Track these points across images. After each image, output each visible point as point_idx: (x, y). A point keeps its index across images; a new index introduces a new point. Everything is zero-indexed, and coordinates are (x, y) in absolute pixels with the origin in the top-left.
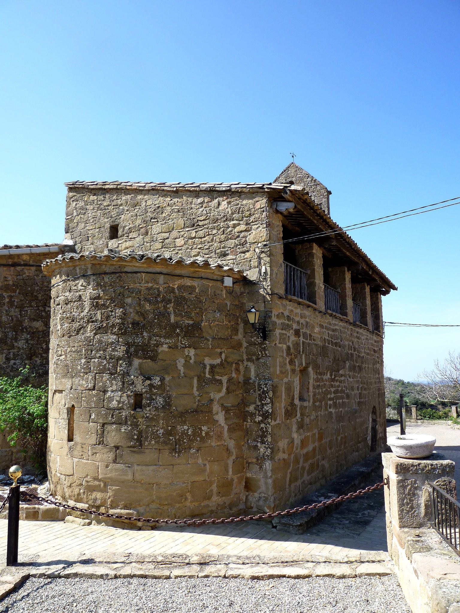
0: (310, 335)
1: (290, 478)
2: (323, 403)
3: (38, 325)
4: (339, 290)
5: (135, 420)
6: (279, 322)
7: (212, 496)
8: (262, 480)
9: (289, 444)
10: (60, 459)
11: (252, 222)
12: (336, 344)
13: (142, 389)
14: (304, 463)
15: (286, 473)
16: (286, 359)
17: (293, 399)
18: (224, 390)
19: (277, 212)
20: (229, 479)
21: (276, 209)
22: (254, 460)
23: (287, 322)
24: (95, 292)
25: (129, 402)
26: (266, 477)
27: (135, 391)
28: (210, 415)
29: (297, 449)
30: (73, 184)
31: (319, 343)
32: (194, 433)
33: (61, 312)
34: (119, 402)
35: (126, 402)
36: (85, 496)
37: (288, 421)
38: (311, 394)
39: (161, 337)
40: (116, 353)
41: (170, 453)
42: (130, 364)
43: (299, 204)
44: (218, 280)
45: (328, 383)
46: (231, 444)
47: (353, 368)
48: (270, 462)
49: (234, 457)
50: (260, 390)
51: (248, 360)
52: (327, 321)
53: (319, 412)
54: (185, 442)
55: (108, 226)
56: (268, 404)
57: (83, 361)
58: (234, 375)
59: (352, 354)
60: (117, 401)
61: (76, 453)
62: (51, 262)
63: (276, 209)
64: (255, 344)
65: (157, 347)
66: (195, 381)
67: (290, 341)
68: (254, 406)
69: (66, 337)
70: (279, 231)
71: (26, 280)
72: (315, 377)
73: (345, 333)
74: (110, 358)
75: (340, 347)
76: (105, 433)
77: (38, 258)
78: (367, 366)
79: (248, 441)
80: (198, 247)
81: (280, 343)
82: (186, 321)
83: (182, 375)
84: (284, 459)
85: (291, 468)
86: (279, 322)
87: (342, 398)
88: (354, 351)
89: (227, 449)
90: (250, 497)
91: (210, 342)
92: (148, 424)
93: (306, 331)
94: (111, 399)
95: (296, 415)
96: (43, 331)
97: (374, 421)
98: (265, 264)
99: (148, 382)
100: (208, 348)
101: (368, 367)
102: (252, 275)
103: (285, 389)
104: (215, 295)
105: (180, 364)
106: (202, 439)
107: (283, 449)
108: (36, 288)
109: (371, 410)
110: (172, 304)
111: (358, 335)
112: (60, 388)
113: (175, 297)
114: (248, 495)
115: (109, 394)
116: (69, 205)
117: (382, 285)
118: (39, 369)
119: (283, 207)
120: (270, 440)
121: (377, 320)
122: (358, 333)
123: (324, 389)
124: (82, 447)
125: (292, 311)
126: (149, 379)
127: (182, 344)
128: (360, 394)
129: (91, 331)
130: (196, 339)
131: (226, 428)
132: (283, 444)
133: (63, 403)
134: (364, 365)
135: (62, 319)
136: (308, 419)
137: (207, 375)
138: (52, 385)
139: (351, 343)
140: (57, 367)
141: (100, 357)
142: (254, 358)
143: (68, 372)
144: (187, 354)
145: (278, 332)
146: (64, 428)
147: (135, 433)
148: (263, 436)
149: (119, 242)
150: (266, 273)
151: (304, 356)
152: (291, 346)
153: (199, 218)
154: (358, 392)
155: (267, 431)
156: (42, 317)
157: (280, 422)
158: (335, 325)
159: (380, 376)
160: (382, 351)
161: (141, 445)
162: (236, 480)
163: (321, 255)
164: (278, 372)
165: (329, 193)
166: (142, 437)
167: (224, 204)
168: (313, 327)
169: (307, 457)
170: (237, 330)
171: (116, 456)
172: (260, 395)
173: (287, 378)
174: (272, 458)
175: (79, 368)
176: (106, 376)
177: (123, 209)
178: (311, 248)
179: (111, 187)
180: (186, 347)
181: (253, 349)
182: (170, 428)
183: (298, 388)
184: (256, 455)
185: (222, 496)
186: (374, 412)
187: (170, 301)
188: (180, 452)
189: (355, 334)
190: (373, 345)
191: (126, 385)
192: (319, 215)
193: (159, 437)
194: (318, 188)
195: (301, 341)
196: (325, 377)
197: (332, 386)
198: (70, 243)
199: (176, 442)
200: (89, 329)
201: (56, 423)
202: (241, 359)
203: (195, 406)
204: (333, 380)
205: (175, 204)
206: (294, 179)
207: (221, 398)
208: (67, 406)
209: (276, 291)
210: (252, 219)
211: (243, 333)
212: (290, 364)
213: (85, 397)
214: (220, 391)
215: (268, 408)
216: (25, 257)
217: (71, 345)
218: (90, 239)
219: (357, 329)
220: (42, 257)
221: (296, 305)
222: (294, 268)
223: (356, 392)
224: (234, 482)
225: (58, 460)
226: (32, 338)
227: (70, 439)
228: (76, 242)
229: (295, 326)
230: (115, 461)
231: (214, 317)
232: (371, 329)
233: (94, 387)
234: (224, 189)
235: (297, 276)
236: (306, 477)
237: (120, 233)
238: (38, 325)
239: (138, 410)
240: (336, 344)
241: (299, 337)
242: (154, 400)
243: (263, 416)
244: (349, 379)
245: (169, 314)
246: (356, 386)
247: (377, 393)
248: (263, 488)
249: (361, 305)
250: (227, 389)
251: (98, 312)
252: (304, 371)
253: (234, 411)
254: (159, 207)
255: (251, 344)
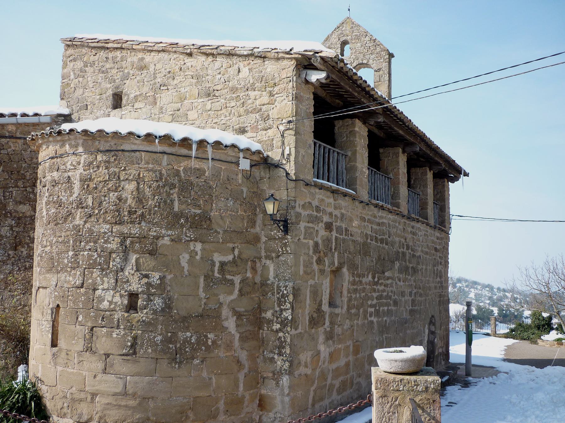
0: (347, 230)
1: (314, 397)
2: (361, 310)
3: (24, 209)
4: (391, 176)
5: (129, 324)
6: (304, 213)
7: (218, 414)
8: (278, 399)
9: (313, 357)
10: (42, 367)
11: (277, 94)
12: (382, 241)
13: (138, 288)
14: (332, 379)
15: (309, 390)
16: (312, 258)
17: (320, 305)
18: (236, 292)
19: (307, 82)
20: (240, 396)
21: (305, 78)
22: (271, 375)
23: (315, 213)
24: (85, 173)
25: (122, 303)
26: (283, 394)
27: (130, 290)
28: (218, 320)
29: (324, 363)
30: (70, 41)
31: (359, 239)
32: (198, 341)
33: (47, 194)
34: (111, 302)
35: (120, 303)
36: (69, 411)
37: (313, 330)
38: (345, 300)
39: (161, 228)
40: (109, 245)
41: (169, 363)
42: (126, 259)
43: (333, 73)
44: (232, 163)
45: (368, 287)
46: (243, 355)
47: (404, 270)
48: (287, 377)
49: (246, 370)
50: (279, 293)
51: (267, 257)
52: (370, 213)
53: (355, 322)
54: (187, 352)
55: (110, 92)
56: (287, 309)
57: (71, 253)
58: (249, 275)
59: (404, 254)
60: (108, 301)
61: (60, 360)
62: (37, 135)
63: (305, 78)
64: (275, 239)
65: (157, 239)
66: (202, 280)
67: (319, 236)
68: (271, 311)
69: (52, 225)
70: (309, 105)
71: (12, 154)
72: (351, 279)
73: (395, 227)
74: (102, 251)
75: (387, 244)
76: (94, 338)
77: (26, 129)
78: (424, 267)
79: (263, 352)
80: (214, 122)
81: (304, 239)
82: (193, 210)
83: (186, 273)
84: (306, 375)
85: (315, 385)
86: (304, 213)
87: (388, 305)
88: (408, 249)
89: (238, 361)
90: (263, 417)
91: (220, 236)
92: (144, 329)
93: (341, 224)
94: (101, 300)
95: (324, 324)
96: (31, 217)
97: (432, 333)
98: (289, 145)
99: (145, 280)
100: (218, 242)
101: (426, 269)
102: (275, 155)
103: (310, 292)
104: (228, 180)
105: (184, 259)
106: (208, 348)
107: (306, 363)
108: (24, 165)
109: (428, 320)
110: (177, 189)
111: (414, 230)
112: (44, 285)
113: (180, 181)
114: (262, 415)
115: (98, 293)
116: (65, 65)
117: (447, 170)
118: (25, 262)
119: (316, 76)
120: (288, 352)
121: (442, 212)
122: (413, 227)
123: (363, 294)
124: (67, 354)
125: (323, 200)
126: (147, 276)
127: (187, 236)
128: (413, 301)
129: (81, 218)
130: (204, 231)
131: (237, 336)
132: (305, 357)
133: (47, 302)
134: (420, 267)
135: (47, 203)
136: (340, 329)
137: (216, 275)
138: (36, 281)
139: (403, 240)
140: (41, 260)
141: (90, 249)
142: (274, 255)
143: (53, 266)
144: (192, 248)
145: (302, 225)
146: (47, 331)
147: (128, 340)
148: (281, 347)
149: (123, 113)
150: (289, 155)
151: (336, 254)
152: (320, 242)
153: (215, 88)
154: (410, 299)
155: (285, 341)
156: (29, 200)
157: (302, 331)
158: (381, 217)
159: (443, 279)
160: (447, 249)
161: (135, 353)
162: (247, 397)
163: (366, 134)
164: (301, 272)
165: (391, 56)
166: (136, 344)
167: (245, 71)
168: (351, 220)
169: (337, 373)
170: (255, 222)
171: (106, 365)
172: (278, 298)
173: (314, 279)
174: (290, 372)
175: (66, 261)
176: (96, 273)
177: (129, 73)
178: (353, 125)
179: (116, 46)
180: (191, 241)
181: (272, 244)
182: (169, 334)
183: (328, 292)
184: (272, 369)
185: (231, 415)
186: (432, 322)
187: (173, 186)
188: (180, 363)
189: (410, 229)
190: (433, 242)
191: (119, 284)
192: (360, 86)
193: (157, 345)
194: (378, 49)
195: (334, 237)
196: (364, 280)
197: (374, 291)
198: (66, 111)
199: (176, 351)
200: (78, 217)
201: (39, 325)
202: (259, 256)
203: (200, 310)
204: (376, 283)
205: (188, 69)
206: (349, 38)
207: (232, 301)
208: (51, 306)
209: (302, 177)
210: (276, 89)
211: (261, 226)
212: (317, 264)
213: (72, 295)
214: (231, 293)
215: (288, 314)
216: (10, 128)
217: (58, 234)
218: (89, 107)
219: (413, 223)
220: (31, 128)
221: (329, 193)
222: (329, 149)
223: (407, 298)
224: (246, 399)
225: (40, 368)
226: (18, 225)
227: (54, 344)
228: (73, 110)
229: (326, 219)
230: (105, 371)
231: (226, 206)
232: (432, 222)
233: (83, 284)
234: (245, 53)
235: (333, 158)
236: (335, 396)
237: (124, 102)
238: (24, 209)
239: (131, 312)
240: (382, 241)
241: (331, 232)
242: (151, 301)
243: (281, 323)
244: (398, 283)
245: (172, 201)
246: (407, 291)
247: (438, 300)
248: (279, 407)
249: (421, 193)
250: (240, 291)
251: (90, 196)
252: (336, 272)
253: (248, 317)
254: (169, 72)
255: (271, 238)
